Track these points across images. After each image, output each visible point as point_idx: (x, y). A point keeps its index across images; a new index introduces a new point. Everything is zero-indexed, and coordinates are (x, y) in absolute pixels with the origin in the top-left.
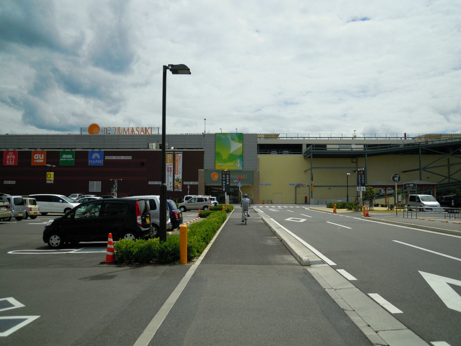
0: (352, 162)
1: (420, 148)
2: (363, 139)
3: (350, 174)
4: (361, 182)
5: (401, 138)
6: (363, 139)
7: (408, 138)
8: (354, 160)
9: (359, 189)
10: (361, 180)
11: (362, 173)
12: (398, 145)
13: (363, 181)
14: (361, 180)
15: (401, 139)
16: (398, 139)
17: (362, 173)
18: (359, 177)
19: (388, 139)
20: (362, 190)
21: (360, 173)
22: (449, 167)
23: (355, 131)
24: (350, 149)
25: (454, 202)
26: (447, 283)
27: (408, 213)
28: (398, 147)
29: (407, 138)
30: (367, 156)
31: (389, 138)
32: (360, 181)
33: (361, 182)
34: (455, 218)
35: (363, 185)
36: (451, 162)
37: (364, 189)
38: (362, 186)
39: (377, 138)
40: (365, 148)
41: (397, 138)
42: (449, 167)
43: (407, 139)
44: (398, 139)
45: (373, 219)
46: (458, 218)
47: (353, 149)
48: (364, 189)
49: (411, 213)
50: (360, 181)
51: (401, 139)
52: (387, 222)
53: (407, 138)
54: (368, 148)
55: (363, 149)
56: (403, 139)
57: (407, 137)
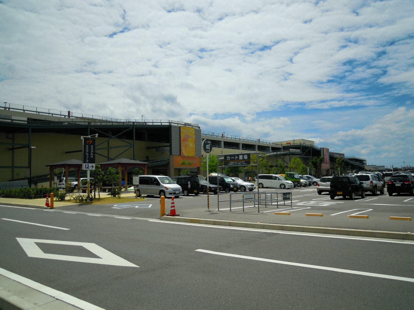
0: (7, 138)
1: (89, 127)
2: (22, 111)
3: (35, 147)
4: (90, 156)
5: (65, 116)
6: (22, 111)
7: (72, 117)
8: (10, 135)
9: (86, 167)
10: (89, 153)
11: (91, 142)
12: (62, 123)
13: (92, 154)
14: (89, 153)
15: (65, 117)
16: (62, 116)
17: (91, 142)
18: (87, 149)
19: (51, 115)
20: (91, 168)
21: (88, 141)
22: (108, 150)
23: (5, 103)
24: (10, 121)
25: (191, 184)
26: (101, 258)
27: (244, 203)
28: (62, 125)
29: (71, 116)
30: (32, 132)
31: (52, 114)
32: (87, 154)
33: (90, 156)
34: (266, 205)
35: (92, 161)
36: (110, 145)
37: (93, 167)
38: (89, 162)
39: (39, 112)
40: (28, 121)
41: (61, 115)
42: (108, 150)
43: (71, 118)
44: (62, 116)
45: (214, 221)
46: (218, 202)
47: (14, 121)
48: (93, 167)
49: (254, 202)
50: (87, 154)
51: (65, 117)
52: (215, 223)
53: (71, 116)
54: (32, 121)
55: (26, 123)
56: (67, 117)
57: (71, 115)
